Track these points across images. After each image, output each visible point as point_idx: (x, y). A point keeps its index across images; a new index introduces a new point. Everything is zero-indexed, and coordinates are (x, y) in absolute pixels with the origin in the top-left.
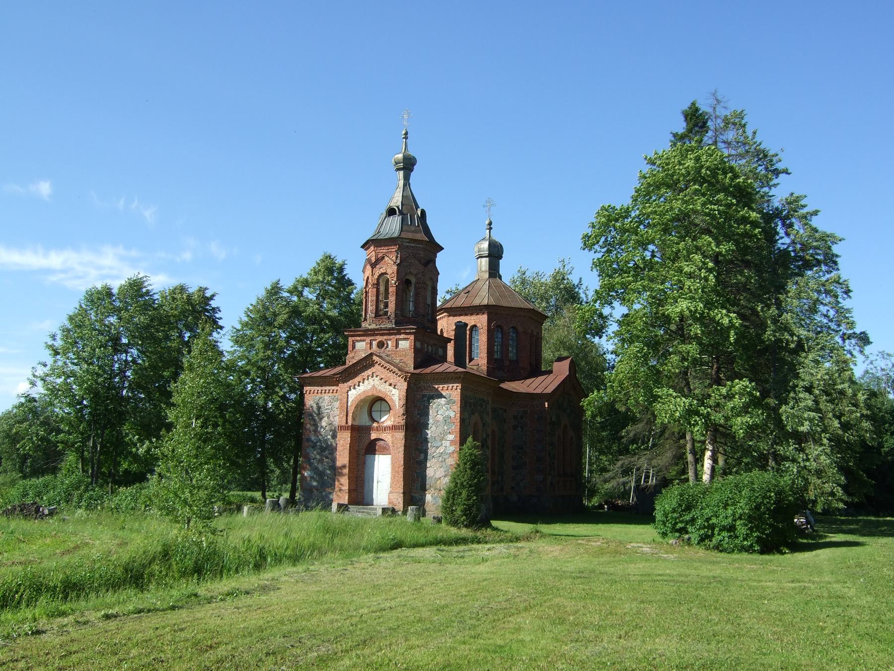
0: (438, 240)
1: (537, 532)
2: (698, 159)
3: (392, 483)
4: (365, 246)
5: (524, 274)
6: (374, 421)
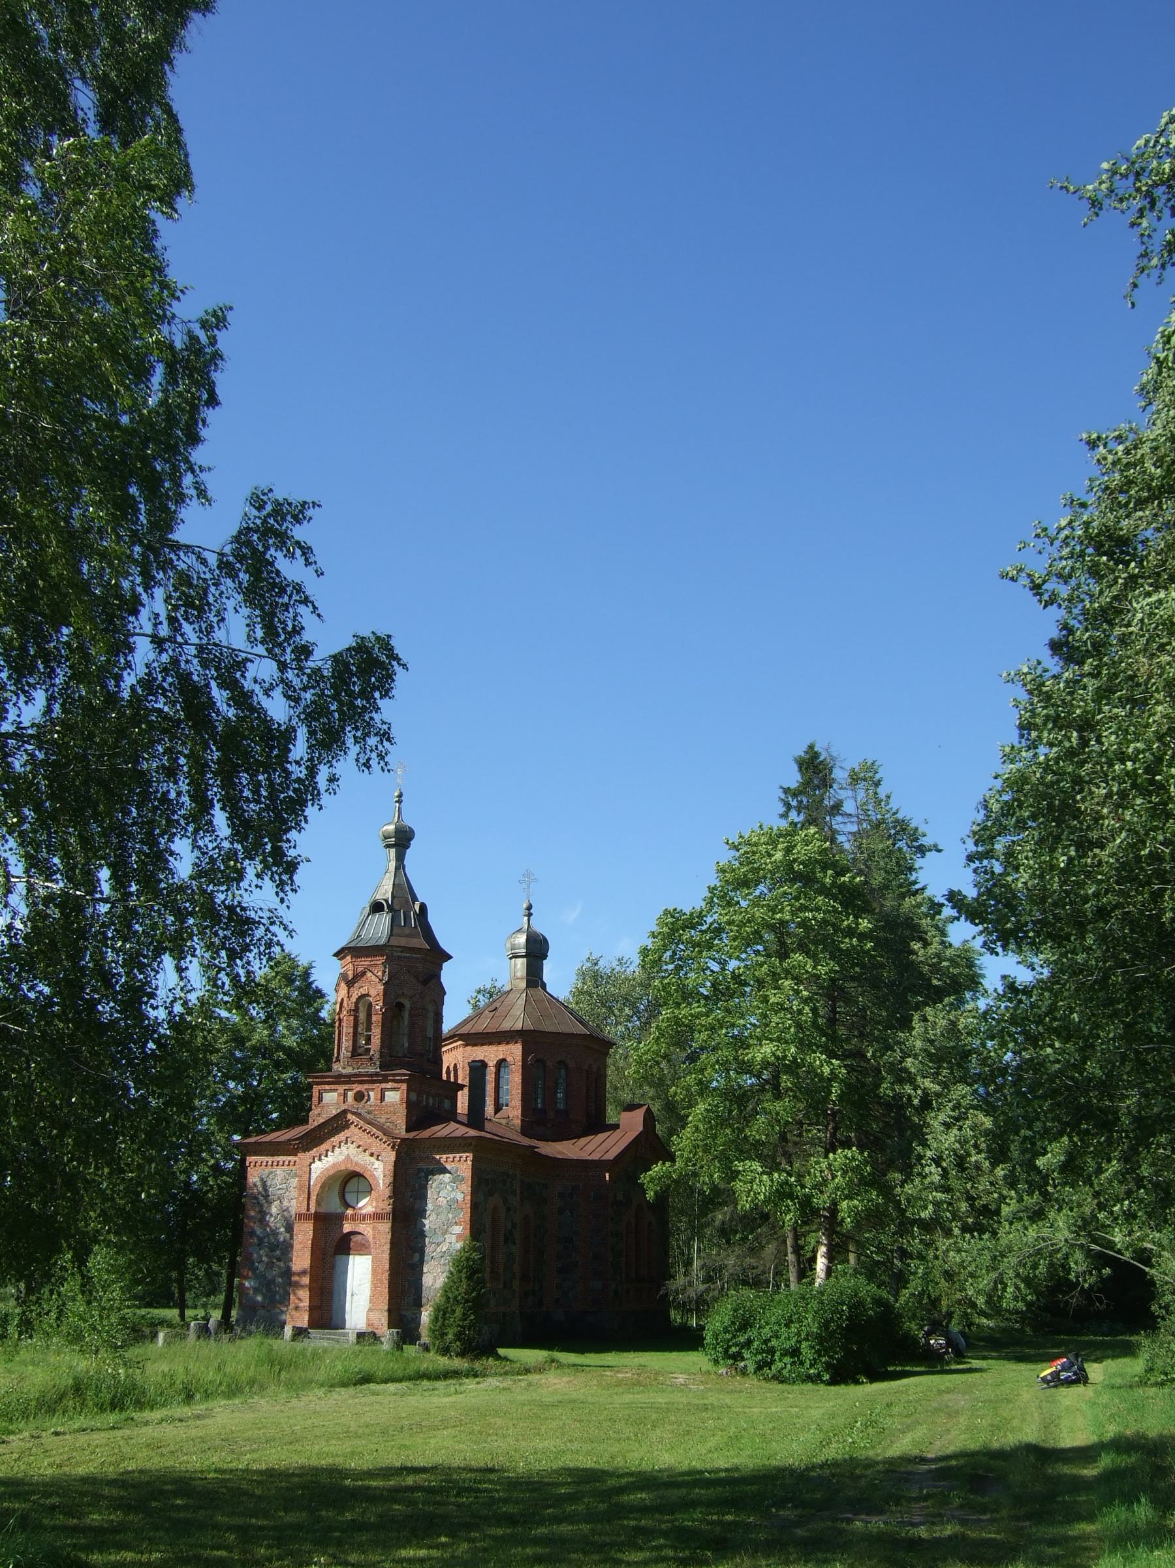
0: (444, 944)
1: (553, 1361)
2: (788, 851)
3: (373, 1295)
4: (340, 954)
5: (596, 964)
6: (347, 1206)
